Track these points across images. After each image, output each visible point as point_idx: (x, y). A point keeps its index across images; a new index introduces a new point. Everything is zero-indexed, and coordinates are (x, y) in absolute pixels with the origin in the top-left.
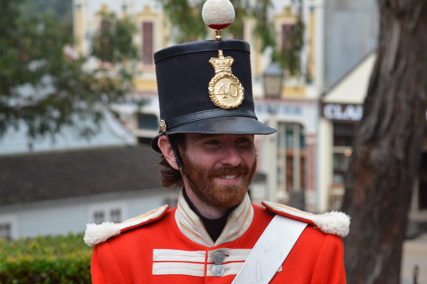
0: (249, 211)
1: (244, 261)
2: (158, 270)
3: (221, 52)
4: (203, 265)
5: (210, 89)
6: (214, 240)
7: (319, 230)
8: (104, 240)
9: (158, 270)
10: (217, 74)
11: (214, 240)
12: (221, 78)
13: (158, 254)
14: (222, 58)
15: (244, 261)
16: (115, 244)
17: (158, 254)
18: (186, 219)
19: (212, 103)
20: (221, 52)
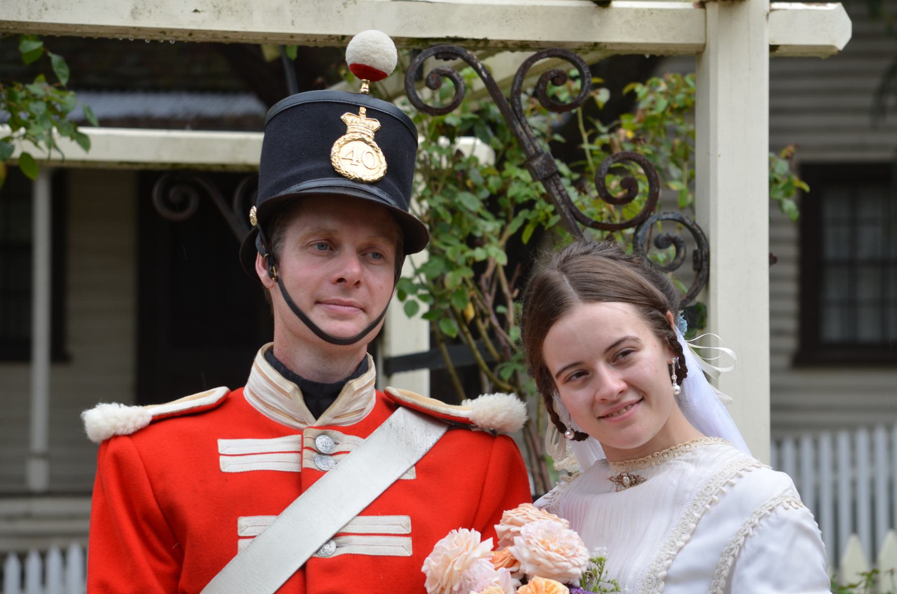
0: (370, 399)
1: (348, 452)
2: (228, 465)
3: (363, 110)
4: (295, 457)
5: (335, 149)
6: (317, 418)
7: (33, 141)
8: (125, 432)
9: (228, 465)
10: (350, 135)
11: (317, 418)
12: (354, 140)
13: (224, 445)
14: (363, 117)
15: (348, 452)
16: (141, 440)
17: (224, 445)
18: (272, 394)
19: (333, 168)
20: (363, 110)
